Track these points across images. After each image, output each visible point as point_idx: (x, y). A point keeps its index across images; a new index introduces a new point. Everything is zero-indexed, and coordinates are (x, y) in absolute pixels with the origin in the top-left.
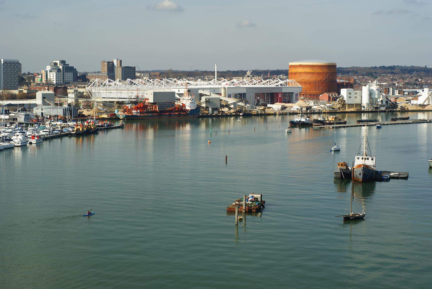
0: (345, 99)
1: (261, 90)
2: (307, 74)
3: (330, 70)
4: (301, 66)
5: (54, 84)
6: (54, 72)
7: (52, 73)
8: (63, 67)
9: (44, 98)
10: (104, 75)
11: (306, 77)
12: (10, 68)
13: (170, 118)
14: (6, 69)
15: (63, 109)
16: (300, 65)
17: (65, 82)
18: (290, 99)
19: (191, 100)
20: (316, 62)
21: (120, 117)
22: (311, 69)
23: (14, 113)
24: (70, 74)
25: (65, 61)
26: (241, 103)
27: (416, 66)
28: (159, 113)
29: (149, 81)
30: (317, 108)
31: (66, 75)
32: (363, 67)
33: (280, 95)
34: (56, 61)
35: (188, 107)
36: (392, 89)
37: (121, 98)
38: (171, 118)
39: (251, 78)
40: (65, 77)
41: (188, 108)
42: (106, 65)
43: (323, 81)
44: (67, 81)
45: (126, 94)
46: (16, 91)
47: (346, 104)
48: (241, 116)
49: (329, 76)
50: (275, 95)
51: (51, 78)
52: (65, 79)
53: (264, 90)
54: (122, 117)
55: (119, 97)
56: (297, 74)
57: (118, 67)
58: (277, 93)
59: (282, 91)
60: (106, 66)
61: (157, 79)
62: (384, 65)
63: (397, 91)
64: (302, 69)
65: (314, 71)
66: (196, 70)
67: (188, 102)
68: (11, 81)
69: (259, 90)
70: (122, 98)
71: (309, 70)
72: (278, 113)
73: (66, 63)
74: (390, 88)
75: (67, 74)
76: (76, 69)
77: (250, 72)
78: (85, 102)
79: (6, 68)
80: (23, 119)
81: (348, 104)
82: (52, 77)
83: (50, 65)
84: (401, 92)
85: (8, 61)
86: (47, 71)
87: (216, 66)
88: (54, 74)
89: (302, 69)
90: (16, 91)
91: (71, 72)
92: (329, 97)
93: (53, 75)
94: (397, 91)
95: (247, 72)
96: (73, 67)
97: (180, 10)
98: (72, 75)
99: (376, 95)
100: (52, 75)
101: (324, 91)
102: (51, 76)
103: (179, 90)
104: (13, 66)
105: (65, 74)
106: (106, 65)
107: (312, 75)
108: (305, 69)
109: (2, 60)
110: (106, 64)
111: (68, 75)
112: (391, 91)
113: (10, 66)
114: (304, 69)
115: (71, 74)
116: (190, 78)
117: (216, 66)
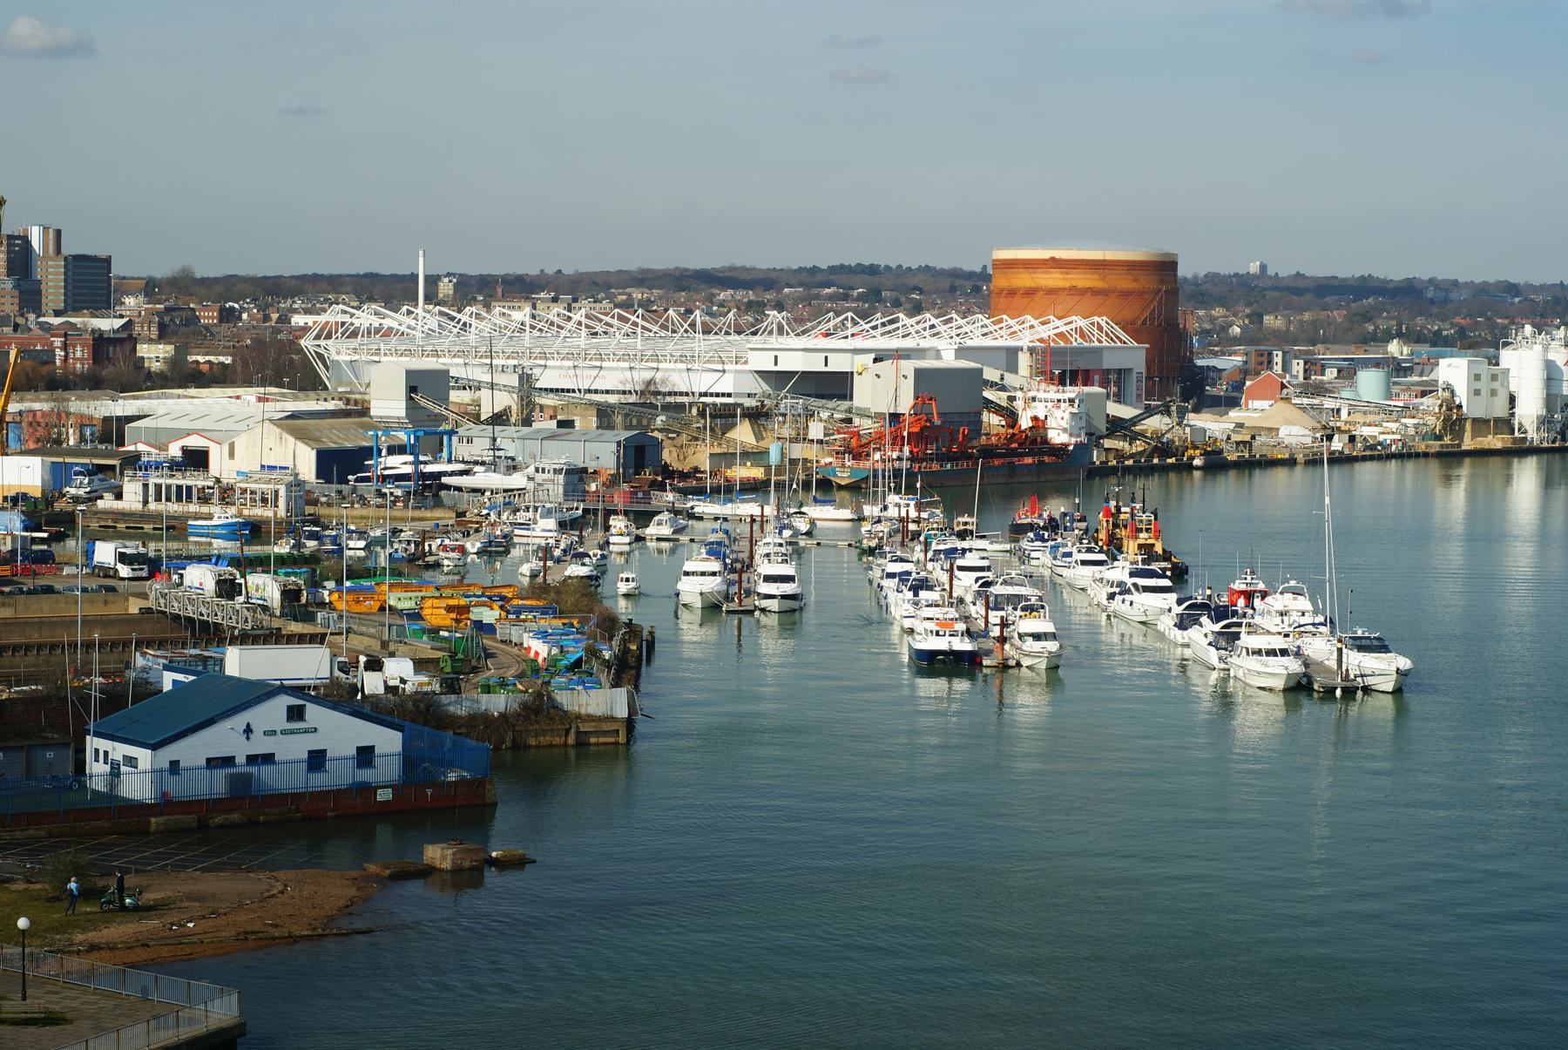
0: (1462, 396)
2: (1078, 298)
3: (1162, 282)
4: (1054, 263)
9: (412, 389)
13: (1010, 481)
15: (619, 443)
16: (1053, 259)
19: (1077, 401)
21: (835, 475)
22: (1096, 276)
29: (413, 313)
30: (1380, 433)
36: (1280, 353)
41: (1057, 437)
43: (1142, 324)
47: (1466, 419)
48: (1198, 468)
49: (1160, 303)
54: (849, 477)
56: (1040, 294)
57: (46, 257)
61: (443, 309)
65: (1106, 286)
67: (1058, 413)
72: (1300, 457)
74: (1275, 353)
77: (450, 281)
80: (561, 490)
81: (1475, 421)
84: (1312, 368)
87: (421, 259)
89: (1061, 277)
97: (82, 48)
103: (776, 357)
108: (1075, 276)
117: (421, 259)
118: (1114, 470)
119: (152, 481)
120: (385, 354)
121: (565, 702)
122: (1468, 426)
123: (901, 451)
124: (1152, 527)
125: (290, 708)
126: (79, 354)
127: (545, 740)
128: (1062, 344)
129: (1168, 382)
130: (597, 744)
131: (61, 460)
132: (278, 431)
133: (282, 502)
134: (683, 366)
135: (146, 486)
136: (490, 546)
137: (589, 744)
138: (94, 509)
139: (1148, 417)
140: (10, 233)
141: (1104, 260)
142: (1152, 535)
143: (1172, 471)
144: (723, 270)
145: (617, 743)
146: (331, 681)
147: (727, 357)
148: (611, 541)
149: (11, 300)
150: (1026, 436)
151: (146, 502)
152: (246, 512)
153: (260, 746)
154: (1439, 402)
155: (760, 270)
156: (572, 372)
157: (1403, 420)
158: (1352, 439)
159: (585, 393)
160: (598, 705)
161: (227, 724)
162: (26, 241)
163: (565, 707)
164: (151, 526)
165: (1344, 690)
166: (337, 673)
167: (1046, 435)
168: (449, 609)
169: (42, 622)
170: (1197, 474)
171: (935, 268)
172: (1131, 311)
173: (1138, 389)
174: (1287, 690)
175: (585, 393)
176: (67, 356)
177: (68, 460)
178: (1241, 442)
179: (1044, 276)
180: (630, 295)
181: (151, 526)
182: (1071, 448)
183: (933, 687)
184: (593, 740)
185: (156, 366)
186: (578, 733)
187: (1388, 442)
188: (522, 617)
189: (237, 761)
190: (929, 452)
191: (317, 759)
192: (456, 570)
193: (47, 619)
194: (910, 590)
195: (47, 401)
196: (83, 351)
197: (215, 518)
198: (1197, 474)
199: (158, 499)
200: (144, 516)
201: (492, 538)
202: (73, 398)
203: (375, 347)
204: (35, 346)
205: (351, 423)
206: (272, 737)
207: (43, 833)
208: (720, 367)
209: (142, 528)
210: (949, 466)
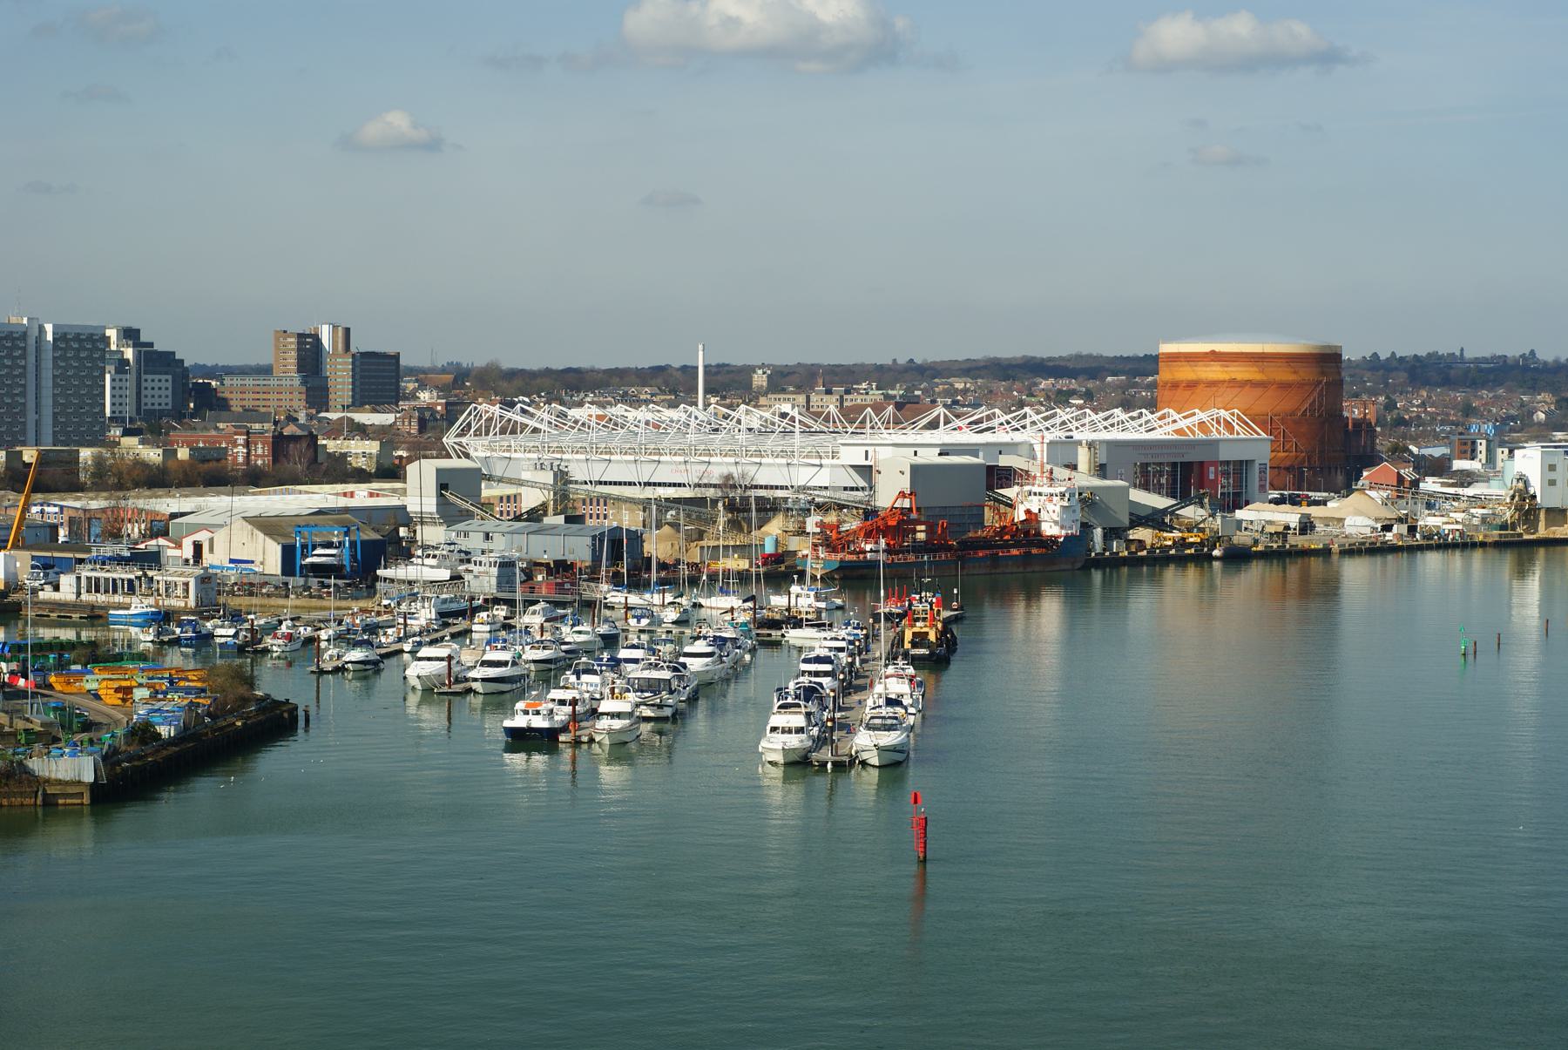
0: (1536, 487)
1: (1151, 451)
3: (1323, 373)
4: (1215, 356)
8: (138, 356)
9: (442, 487)
10: (289, 383)
11: (1236, 399)
12: (76, 357)
13: (993, 571)
15: (594, 538)
16: (1213, 352)
17: (144, 410)
18: (1241, 486)
19: (1067, 495)
20: (1275, 343)
22: (1255, 369)
23: (434, 557)
24: (149, 381)
25: (138, 331)
26: (1192, 507)
27: (1112, 356)
28: (956, 551)
30: (1444, 523)
31: (149, 384)
32: (1111, 354)
33: (1212, 469)
35: (1052, 524)
36: (1484, 442)
37: (605, 483)
38: (997, 571)
39: (842, 397)
40: (144, 392)
41: (1049, 529)
42: (293, 346)
44: (149, 407)
45: (629, 465)
46: (152, 454)
47: (1539, 509)
48: (1217, 558)
49: (1320, 395)
50: (1196, 469)
52: (144, 400)
53: (1165, 451)
55: (646, 481)
57: (335, 354)
58: (1202, 463)
59: (1218, 454)
60: (293, 349)
62: (1499, 353)
63: (1503, 452)
64: (1219, 368)
65: (1265, 378)
66: (452, 363)
67: (1050, 507)
68: (81, 411)
69: (1148, 452)
70: (610, 483)
71: (1246, 371)
73: (143, 338)
74: (1479, 441)
75: (160, 381)
76: (182, 361)
77: (764, 373)
78: (595, 503)
79: (63, 358)
80: (494, 581)
81: (1549, 510)
85: (69, 331)
87: (701, 353)
90: (152, 454)
91: (166, 373)
92: (1398, 477)
94: (1503, 452)
95: (755, 372)
96: (174, 353)
97: (433, 145)
98: (169, 385)
101: (1303, 454)
105: (146, 380)
106: (293, 346)
107: (1259, 391)
109: (49, 328)
110: (291, 343)
111: (156, 384)
112: (1481, 452)
113: (78, 350)
114: (1226, 369)
115: (167, 381)
116: (586, 395)
117: (701, 353)
118: (1124, 561)
119: (84, 574)
120: (515, 451)
121: (36, 768)
122: (1542, 516)
123: (876, 543)
124: (928, 616)
126: (260, 451)
127: (17, 801)
128: (1204, 437)
129: (1330, 472)
130: (65, 805)
132: (250, 527)
134: (784, 461)
135: (79, 578)
136: (349, 634)
137: (57, 805)
139: (1183, 507)
140: (302, 332)
141: (1263, 353)
142: (928, 624)
143: (1191, 562)
144: (1069, 359)
145: (82, 804)
147: (824, 452)
148: (473, 629)
149: (299, 396)
150: (1017, 528)
151: (79, 594)
154: (1512, 492)
155: (1107, 357)
156: (683, 467)
157: (1472, 511)
158: (1412, 530)
159: (596, 485)
160: (66, 771)
162: (317, 339)
164: (78, 615)
165: (835, 764)
167: (1040, 527)
168: (117, 690)
170: (1216, 564)
171: (1151, 355)
172: (1267, 403)
173: (1261, 480)
174: (787, 764)
175: (596, 485)
176: (248, 453)
178: (1276, 533)
179: (1204, 369)
180: (952, 385)
181: (78, 615)
182: (1062, 539)
183: (518, 759)
184: (61, 801)
185: (361, 463)
186: (45, 795)
187: (1446, 532)
188: (169, 696)
190: (906, 544)
192: (283, 655)
194: (573, 674)
195: (106, 499)
196: (263, 448)
197: (133, 608)
198: (1216, 564)
199: (89, 591)
200: (74, 607)
201: (350, 627)
202: (178, 495)
203: (506, 444)
204: (220, 444)
205: (328, 519)
208: (817, 462)
209: (71, 617)
210: (926, 558)
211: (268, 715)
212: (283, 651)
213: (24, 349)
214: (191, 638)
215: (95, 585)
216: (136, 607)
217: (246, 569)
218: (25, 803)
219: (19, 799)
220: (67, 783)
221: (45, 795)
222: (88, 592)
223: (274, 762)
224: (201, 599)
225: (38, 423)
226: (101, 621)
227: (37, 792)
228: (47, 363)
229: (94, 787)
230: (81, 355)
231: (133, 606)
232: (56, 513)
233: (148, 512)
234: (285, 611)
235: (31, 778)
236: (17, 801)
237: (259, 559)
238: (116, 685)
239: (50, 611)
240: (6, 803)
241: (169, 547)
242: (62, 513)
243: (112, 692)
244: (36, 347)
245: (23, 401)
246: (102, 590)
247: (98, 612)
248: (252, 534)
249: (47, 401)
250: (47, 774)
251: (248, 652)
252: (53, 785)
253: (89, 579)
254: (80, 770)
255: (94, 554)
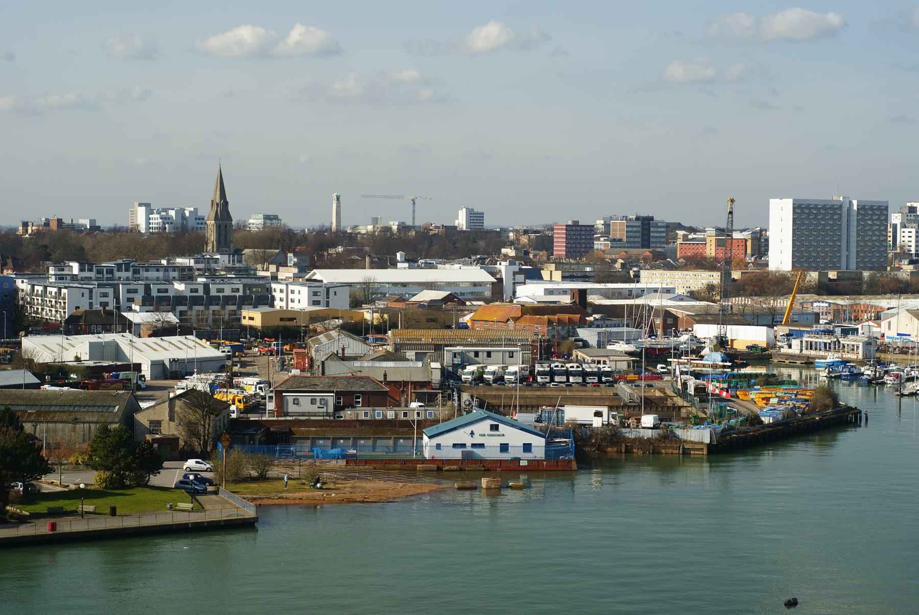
5: (912, 254)
6: (912, 228)
7: (906, 230)
14: (863, 223)
34: (913, 203)
51: (904, 241)
76: (99, 227)
82: (906, 239)
83: (899, 213)
86: (896, 225)
88: (911, 232)
93: (910, 234)
99: (484, 486)
100: (907, 234)
102: (904, 237)
104: (869, 214)
109: (855, 202)
113: (872, 215)
121: (680, 435)
122: (205, 302)
125: (492, 426)
130: (694, 454)
131: (798, 329)
132: (910, 315)
133: (861, 350)
137: (690, 454)
138: (779, 353)
145: (703, 454)
146: (608, 423)
151: (801, 350)
152: (844, 356)
153: (477, 440)
161: (462, 431)
163: (680, 437)
164: (800, 362)
166: (258, 391)
168: (763, 399)
169: (581, 398)
177: (802, 329)
181: (800, 362)
184: (692, 452)
186: (684, 448)
189: (467, 445)
191: (504, 448)
192: (893, 386)
193: (584, 396)
197: (828, 359)
199: (807, 349)
200: (798, 357)
206: (484, 437)
207: (371, 467)
209: (796, 363)
211: (839, 415)
212: (893, 384)
213: (840, 215)
214: (847, 375)
215: (810, 346)
216: (830, 358)
217: (906, 339)
218: (674, 452)
219: (671, 450)
220: (695, 443)
221: (684, 448)
222: (806, 349)
223: (848, 439)
224: (866, 354)
225: (848, 257)
226: (812, 365)
227: (680, 447)
228: (854, 223)
229: (710, 446)
230: (874, 218)
231: (828, 357)
232: (827, 307)
233: (875, 307)
234: (913, 362)
235: (677, 440)
236: (670, 451)
237: (913, 334)
238: (764, 396)
239: (786, 359)
240: (664, 452)
241: (874, 326)
242: (830, 307)
243: (760, 399)
244: (848, 214)
245: (839, 244)
246: (813, 348)
247: (811, 360)
248: (911, 319)
249: (853, 244)
250: (686, 438)
251: (873, 383)
252: (688, 443)
253: (807, 342)
254: (702, 436)
255: (815, 329)
